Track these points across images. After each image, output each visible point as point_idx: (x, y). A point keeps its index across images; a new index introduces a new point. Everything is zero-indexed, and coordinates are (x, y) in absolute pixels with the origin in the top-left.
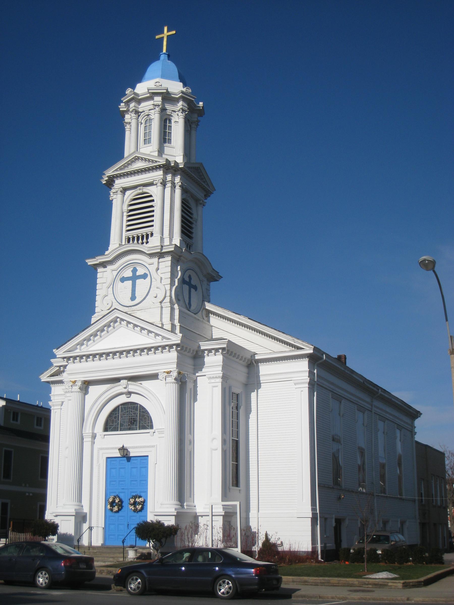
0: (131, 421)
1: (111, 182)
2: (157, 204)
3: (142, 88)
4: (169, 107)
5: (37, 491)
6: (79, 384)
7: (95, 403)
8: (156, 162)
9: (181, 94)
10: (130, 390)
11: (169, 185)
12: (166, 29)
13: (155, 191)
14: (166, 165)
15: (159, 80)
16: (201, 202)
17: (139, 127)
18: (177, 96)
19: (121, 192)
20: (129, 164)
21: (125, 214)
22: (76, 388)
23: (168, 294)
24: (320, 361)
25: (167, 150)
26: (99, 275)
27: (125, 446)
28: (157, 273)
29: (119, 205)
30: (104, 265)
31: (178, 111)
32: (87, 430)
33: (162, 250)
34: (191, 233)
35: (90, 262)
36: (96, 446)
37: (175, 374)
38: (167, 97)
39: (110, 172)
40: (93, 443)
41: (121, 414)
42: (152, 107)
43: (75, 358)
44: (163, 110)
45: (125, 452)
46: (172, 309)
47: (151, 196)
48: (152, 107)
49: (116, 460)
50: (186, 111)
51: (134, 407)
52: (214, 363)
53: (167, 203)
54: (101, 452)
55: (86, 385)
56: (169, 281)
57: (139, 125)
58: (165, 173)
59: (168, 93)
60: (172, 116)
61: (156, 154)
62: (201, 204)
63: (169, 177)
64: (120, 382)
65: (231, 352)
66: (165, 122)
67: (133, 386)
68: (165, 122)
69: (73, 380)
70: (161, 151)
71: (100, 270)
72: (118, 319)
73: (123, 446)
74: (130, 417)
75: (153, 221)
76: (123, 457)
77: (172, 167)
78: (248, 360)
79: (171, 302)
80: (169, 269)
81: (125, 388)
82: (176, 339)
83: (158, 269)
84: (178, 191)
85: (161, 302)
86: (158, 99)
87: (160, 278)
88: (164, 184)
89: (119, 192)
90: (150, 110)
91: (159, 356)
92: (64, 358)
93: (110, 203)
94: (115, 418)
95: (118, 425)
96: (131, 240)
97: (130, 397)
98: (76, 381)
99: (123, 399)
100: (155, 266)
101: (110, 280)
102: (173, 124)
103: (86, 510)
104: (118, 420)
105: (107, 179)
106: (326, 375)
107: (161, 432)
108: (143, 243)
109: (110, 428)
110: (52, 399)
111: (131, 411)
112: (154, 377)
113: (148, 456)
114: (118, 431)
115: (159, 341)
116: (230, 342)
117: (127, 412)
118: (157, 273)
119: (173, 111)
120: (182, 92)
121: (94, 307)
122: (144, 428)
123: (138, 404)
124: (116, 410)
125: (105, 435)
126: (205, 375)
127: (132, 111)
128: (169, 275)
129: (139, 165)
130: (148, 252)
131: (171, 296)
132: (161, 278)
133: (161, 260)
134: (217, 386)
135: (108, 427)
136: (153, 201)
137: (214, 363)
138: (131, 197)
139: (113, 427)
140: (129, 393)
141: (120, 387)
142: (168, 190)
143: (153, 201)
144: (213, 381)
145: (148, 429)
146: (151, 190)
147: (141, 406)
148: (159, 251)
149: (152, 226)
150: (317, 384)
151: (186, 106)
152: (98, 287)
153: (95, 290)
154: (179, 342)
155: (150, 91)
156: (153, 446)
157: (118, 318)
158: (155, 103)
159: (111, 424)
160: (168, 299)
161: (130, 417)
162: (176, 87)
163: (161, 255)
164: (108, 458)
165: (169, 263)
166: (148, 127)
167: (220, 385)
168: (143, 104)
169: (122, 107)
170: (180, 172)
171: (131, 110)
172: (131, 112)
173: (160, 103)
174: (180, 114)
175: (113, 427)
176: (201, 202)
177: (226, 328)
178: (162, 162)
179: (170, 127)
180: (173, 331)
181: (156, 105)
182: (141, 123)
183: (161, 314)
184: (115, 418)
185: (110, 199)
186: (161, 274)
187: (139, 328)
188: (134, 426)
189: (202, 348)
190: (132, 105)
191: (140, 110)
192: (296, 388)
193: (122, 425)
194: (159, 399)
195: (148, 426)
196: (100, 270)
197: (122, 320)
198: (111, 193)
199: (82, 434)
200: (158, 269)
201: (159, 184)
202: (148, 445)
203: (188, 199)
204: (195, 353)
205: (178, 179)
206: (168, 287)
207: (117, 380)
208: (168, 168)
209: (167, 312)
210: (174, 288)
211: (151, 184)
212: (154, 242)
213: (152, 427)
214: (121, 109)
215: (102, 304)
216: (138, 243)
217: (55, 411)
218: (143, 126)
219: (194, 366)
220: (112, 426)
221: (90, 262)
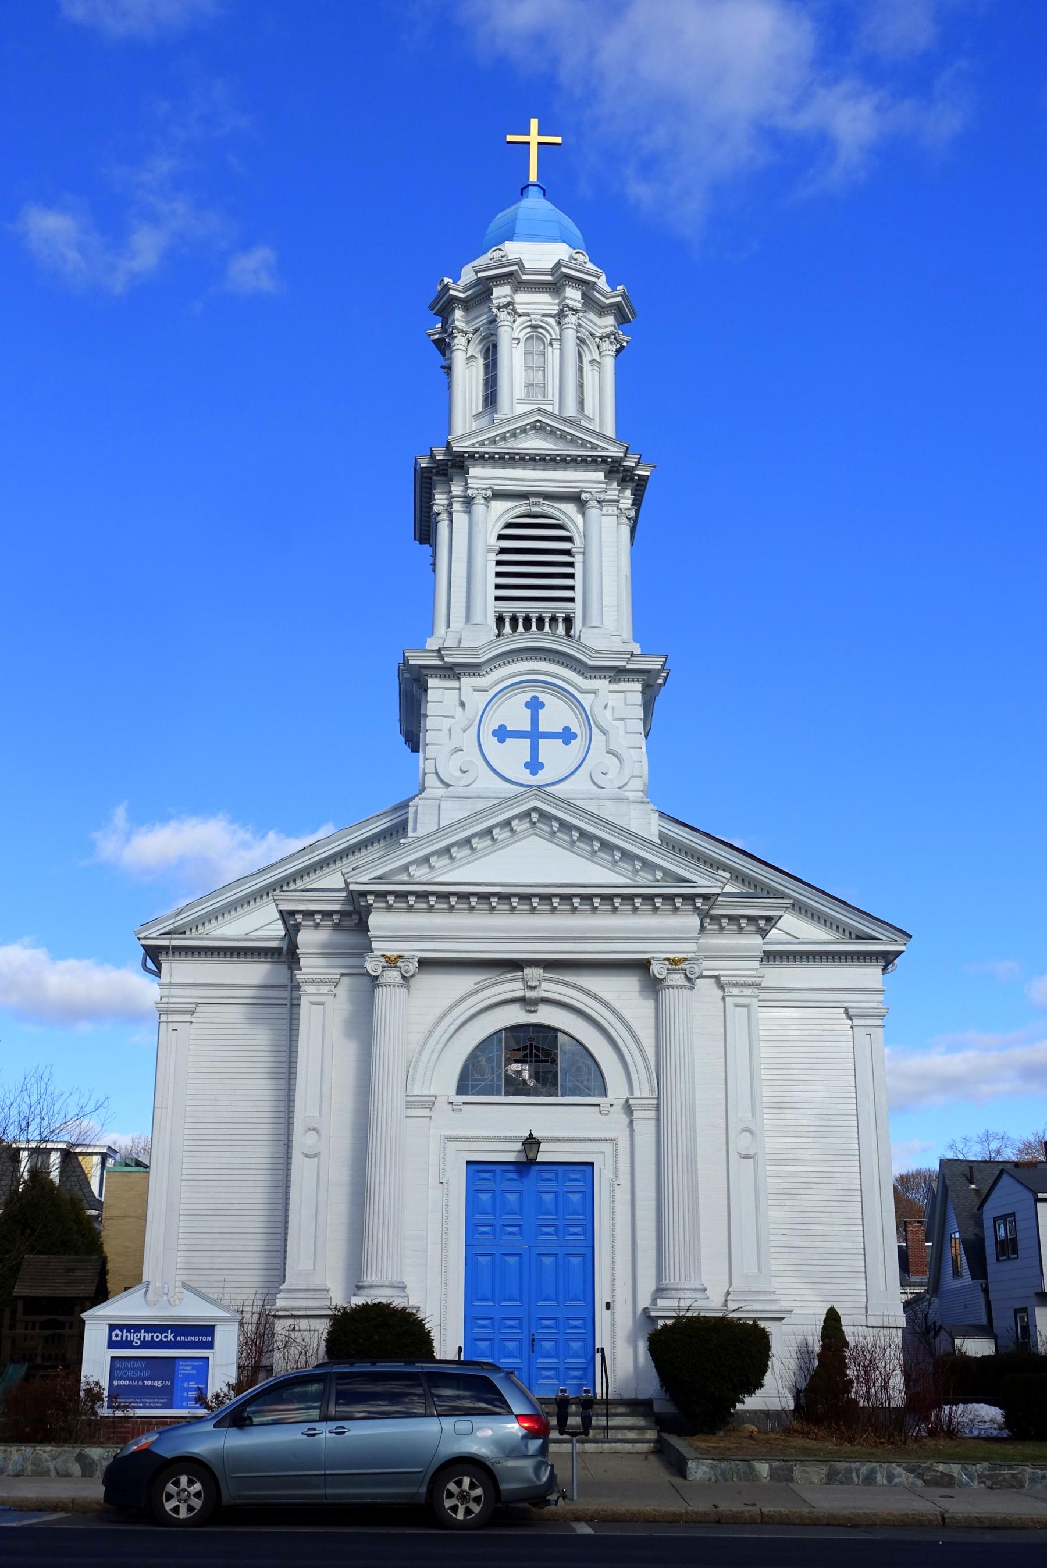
8: (594, 447)
9: (620, 299)
12: (534, 123)
18: (608, 301)
20: (514, 435)
26: (431, 695)
54: (453, 1146)
67: (550, 989)
73: (531, 1135)
82: (710, 884)
96: (521, 625)
97: (535, 1011)
99: (515, 1016)
109: (473, 1087)
115: (645, 883)
123: (556, 1030)
135: (471, 1081)
138: (507, 518)
139: (483, 1084)
141: (512, 987)
155: (480, 275)
164: (468, 1163)
175: (483, 1084)
216: (570, 636)
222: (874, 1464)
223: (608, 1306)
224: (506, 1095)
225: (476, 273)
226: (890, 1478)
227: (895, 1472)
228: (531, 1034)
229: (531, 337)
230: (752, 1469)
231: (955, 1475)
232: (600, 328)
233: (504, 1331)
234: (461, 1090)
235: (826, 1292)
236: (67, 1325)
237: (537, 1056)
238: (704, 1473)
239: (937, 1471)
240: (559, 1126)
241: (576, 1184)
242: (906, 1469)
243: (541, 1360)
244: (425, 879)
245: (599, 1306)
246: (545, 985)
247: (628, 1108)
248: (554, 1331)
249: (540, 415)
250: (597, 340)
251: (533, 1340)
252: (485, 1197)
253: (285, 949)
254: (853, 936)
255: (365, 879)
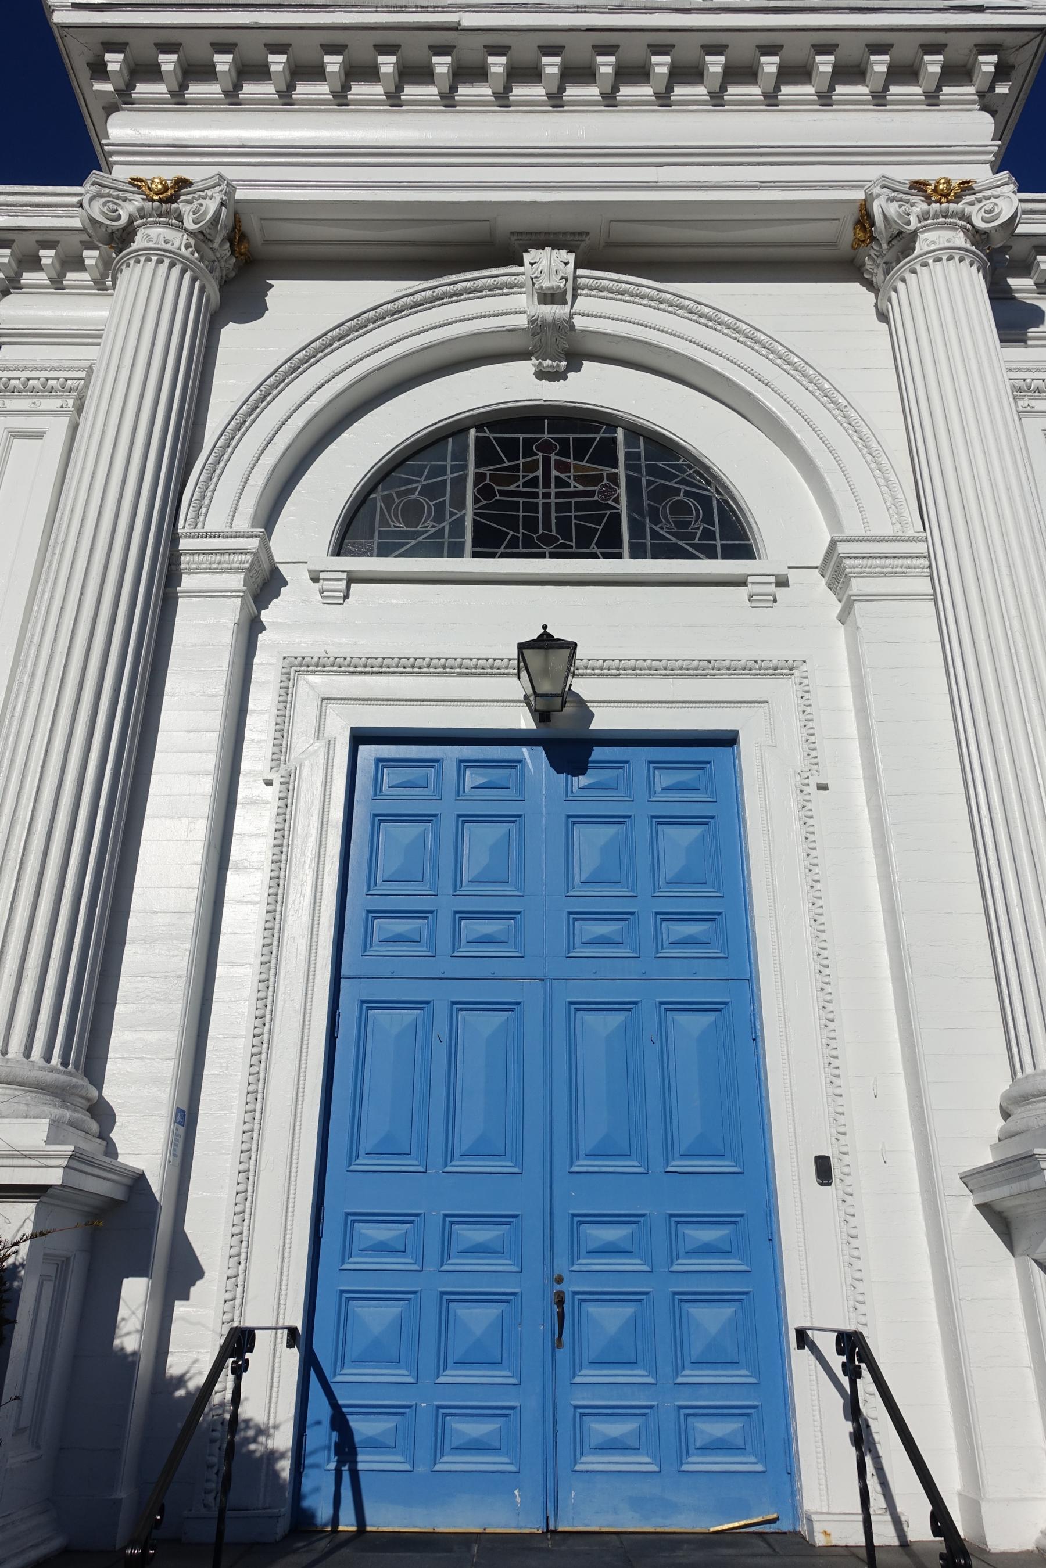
5: (719, 555)
32: (223, 507)
41: (479, 478)
55: (242, 263)
67: (607, 308)
99: (513, 385)
103: (141, 1145)
104: (461, 504)
111: (564, 467)
113: (728, 740)
125: (352, 579)
141: (500, 304)
147: (636, 431)
199: (174, 539)
202: (744, 653)
223: (824, 1170)
228: (546, 436)
233: (685, 1264)
236: (558, 1287)
240: (635, 633)
243: (588, 1375)
245: (791, 1173)
247: (836, 570)
248: (633, 1264)
251: (560, 1302)
253: (57, 1112)
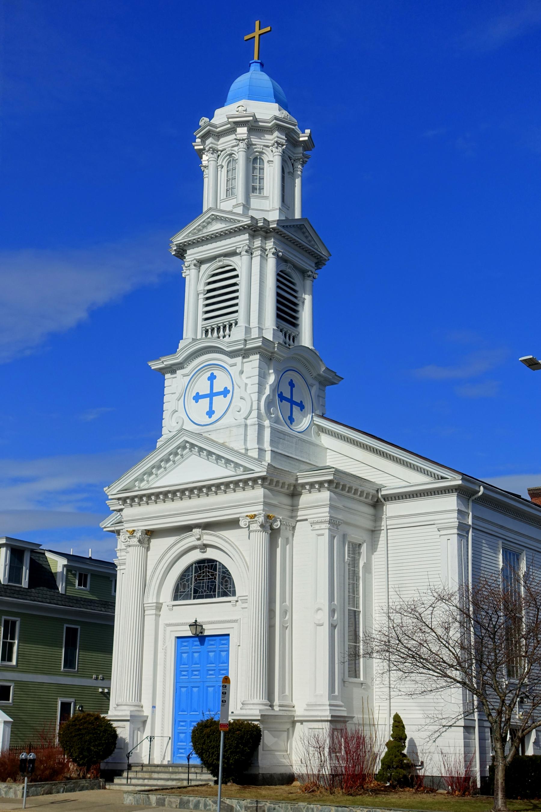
0: (208, 585)
1: (181, 253)
2: (242, 281)
3: (221, 116)
4: (258, 142)
6: (138, 534)
7: (160, 561)
10: (205, 542)
11: (258, 253)
13: (239, 263)
14: (252, 226)
15: (251, 103)
16: (310, 273)
17: (219, 172)
18: (270, 125)
19: (195, 265)
21: (201, 296)
22: (135, 541)
23: (255, 406)
24: (476, 496)
25: (255, 203)
26: (167, 383)
27: (198, 621)
28: (241, 377)
29: (195, 284)
30: (172, 369)
31: (272, 146)
32: (151, 599)
33: (245, 345)
34: (296, 318)
35: (155, 365)
36: (162, 621)
37: (261, 519)
38: (255, 127)
39: (180, 238)
40: (158, 616)
41: (195, 576)
42: (234, 143)
43: (132, 499)
44: (250, 145)
45: (199, 629)
46: (261, 427)
47: (234, 270)
48: (234, 143)
49: (215, 640)
50: (283, 145)
51: (212, 565)
52: (315, 505)
53: (257, 275)
54: (169, 629)
56: (256, 388)
57: (219, 169)
58: (253, 236)
59: (256, 120)
60: (263, 153)
61: (240, 210)
62: (309, 276)
63: (258, 243)
64: (192, 531)
65: (341, 485)
66: (254, 160)
67: (208, 538)
68: (254, 160)
69: (131, 529)
70: (247, 206)
71: (167, 376)
72: (187, 445)
73: (196, 621)
74: (206, 580)
75: (236, 305)
76: (196, 636)
77: (261, 228)
78: (373, 496)
79: (259, 416)
80: (256, 371)
81: (199, 539)
83: (242, 372)
84: (271, 262)
85: (246, 419)
86: (242, 131)
87: (246, 383)
88: (250, 252)
89: (192, 267)
90: (233, 147)
91: (240, 495)
92: (119, 499)
93: (183, 281)
94: (187, 581)
95: (191, 591)
97: (206, 552)
98: (134, 531)
100: (239, 367)
101: (179, 390)
102: (266, 165)
104: (191, 584)
105: (175, 248)
106: (488, 514)
107: (245, 601)
108: (224, 337)
109: (181, 595)
110: (118, 555)
111: (209, 572)
112: (233, 524)
113: (228, 635)
114: (190, 599)
116: (337, 472)
117: (203, 573)
118: (241, 377)
119: (264, 146)
120: (276, 118)
121: (160, 427)
122: (225, 594)
123: (217, 561)
124: (188, 569)
126: (306, 520)
127: (209, 150)
128: (256, 380)
129: (217, 227)
130: (227, 350)
131: (259, 409)
132: (246, 384)
133: (245, 360)
134: (323, 535)
135: (179, 593)
136: (237, 276)
137: (315, 505)
140: (205, 546)
141: (190, 540)
142: (256, 260)
143: (237, 276)
144: (317, 527)
145: (230, 596)
146: (235, 261)
148: (242, 346)
149: (236, 312)
150: (473, 528)
151: (284, 137)
152: (166, 399)
153: (161, 403)
154: (265, 474)
155: (230, 120)
156: (235, 621)
157: (187, 442)
158: (239, 137)
159: (182, 590)
160: (254, 414)
161: (206, 580)
162: (268, 111)
163: (245, 353)
164: (178, 638)
165: (256, 363)
166: (231, 171)
167: (326, 532)
168: (222, 140)
169: (198, 145)
170: (272, 234)
171: (207, 148)
172: (207, 151)
173: (245, 136)
174: (274, 150)
176: (310, 273)
177: (340, 452)
178: (246, 221)
179: (262, 169)
180: (260, 459)
181: (240, 140)
182: (222, 167)
183: (246, 435)
184: (187, 581)
185: (183, 276)
186: (247, 378)
187: (214, 456)
188: (212, 593)
189: (299, 482)
190: (209, 141)
191: (220, 148)
192: (440, 535)
193: (196, 591)
194: (241, 554)
195: (230, 591)
196: (167, 376)
197: (193, 446)
198: (184, 268)
200: (242, 372)
201: (244, 253)
203: (288, 270)
204: (292, 488)
205: (270, 245)
206: (255, 397)
207: (188, 528)
208: (256, 230)
209: (253, 432)
210: (264, 398)
211: (233, 254)
212: (238, 334)
213: (234, 594)
214: (196, 148)
215: (170, 424)
217: (122, 571)
218: (225, 170)
219: (292, 506)
220: (185, 592)
221: (155, 365)
222: (199, 798)
224: (194, 599)
225: (228, 118)
226: (206, 805)
227: (208, 803)
229: (230, 161)
230: (148, 798)
231: (234, 806)
232: (272, 140)
234: (176, 598)
235: (422, 704)
237: (208, 576)
238: (130, 800)
239: (225, 803)
240: (210, 613)
241: (186, 648)
242: (213, 802)
244: (146, 487)
246: (205, 537)
249: (212, 211)
250: (292, 161)
252: (185, 655)
254: (440, 478)
255: (115, 492)
